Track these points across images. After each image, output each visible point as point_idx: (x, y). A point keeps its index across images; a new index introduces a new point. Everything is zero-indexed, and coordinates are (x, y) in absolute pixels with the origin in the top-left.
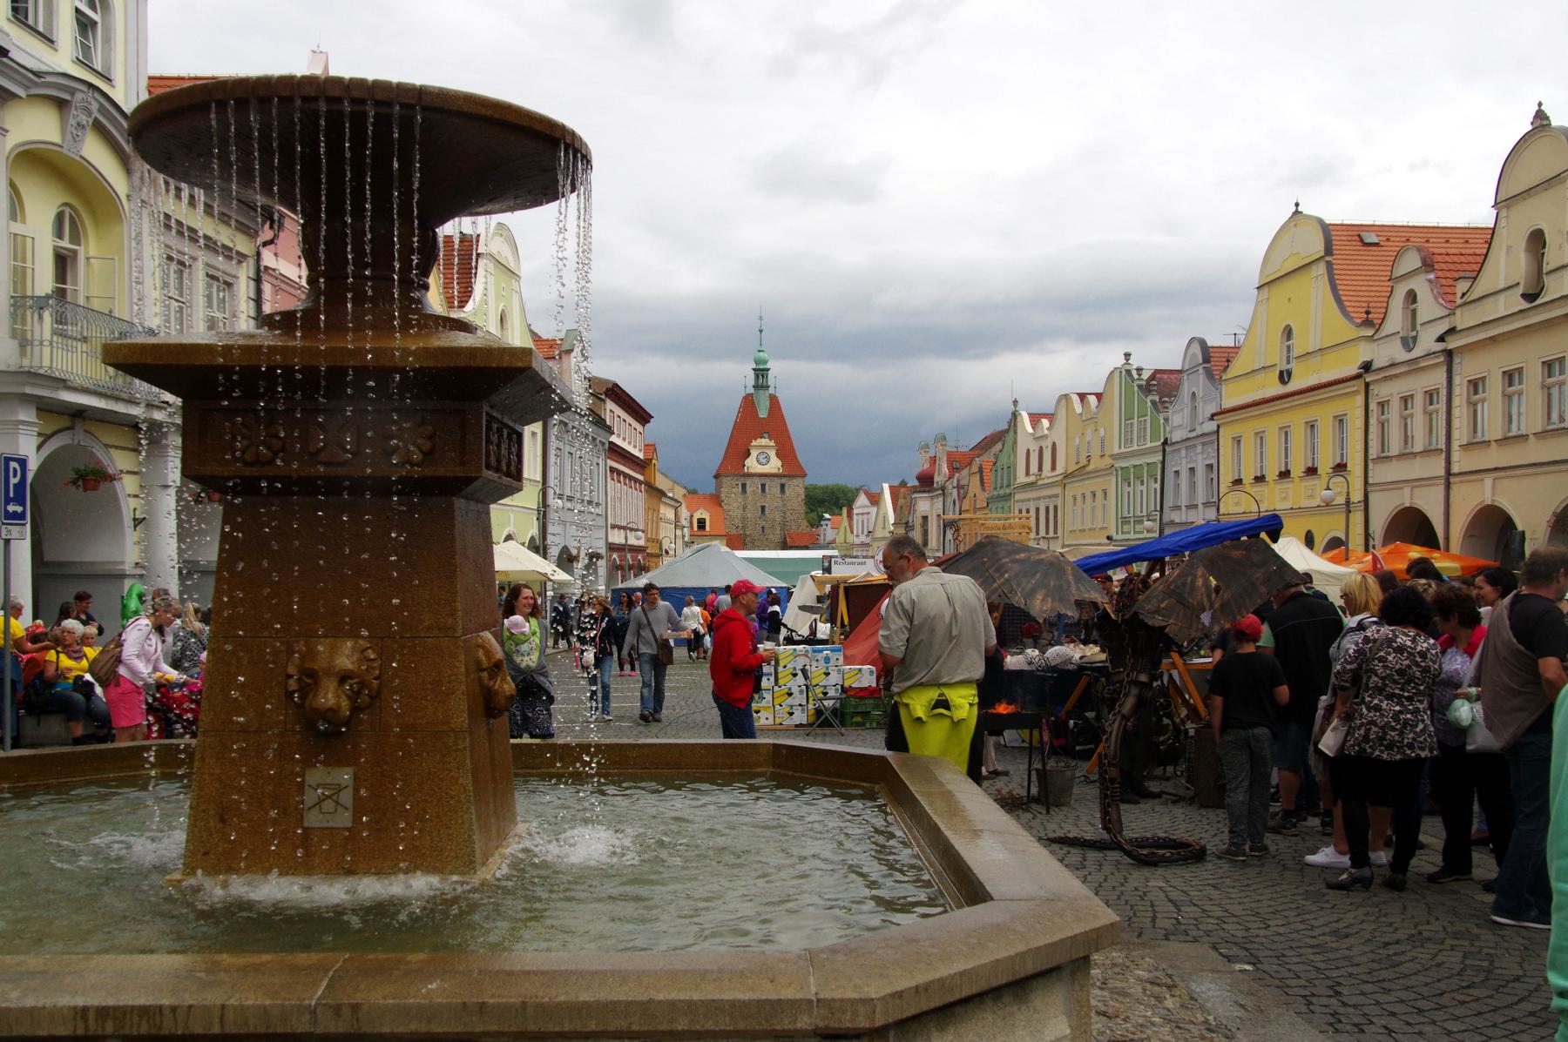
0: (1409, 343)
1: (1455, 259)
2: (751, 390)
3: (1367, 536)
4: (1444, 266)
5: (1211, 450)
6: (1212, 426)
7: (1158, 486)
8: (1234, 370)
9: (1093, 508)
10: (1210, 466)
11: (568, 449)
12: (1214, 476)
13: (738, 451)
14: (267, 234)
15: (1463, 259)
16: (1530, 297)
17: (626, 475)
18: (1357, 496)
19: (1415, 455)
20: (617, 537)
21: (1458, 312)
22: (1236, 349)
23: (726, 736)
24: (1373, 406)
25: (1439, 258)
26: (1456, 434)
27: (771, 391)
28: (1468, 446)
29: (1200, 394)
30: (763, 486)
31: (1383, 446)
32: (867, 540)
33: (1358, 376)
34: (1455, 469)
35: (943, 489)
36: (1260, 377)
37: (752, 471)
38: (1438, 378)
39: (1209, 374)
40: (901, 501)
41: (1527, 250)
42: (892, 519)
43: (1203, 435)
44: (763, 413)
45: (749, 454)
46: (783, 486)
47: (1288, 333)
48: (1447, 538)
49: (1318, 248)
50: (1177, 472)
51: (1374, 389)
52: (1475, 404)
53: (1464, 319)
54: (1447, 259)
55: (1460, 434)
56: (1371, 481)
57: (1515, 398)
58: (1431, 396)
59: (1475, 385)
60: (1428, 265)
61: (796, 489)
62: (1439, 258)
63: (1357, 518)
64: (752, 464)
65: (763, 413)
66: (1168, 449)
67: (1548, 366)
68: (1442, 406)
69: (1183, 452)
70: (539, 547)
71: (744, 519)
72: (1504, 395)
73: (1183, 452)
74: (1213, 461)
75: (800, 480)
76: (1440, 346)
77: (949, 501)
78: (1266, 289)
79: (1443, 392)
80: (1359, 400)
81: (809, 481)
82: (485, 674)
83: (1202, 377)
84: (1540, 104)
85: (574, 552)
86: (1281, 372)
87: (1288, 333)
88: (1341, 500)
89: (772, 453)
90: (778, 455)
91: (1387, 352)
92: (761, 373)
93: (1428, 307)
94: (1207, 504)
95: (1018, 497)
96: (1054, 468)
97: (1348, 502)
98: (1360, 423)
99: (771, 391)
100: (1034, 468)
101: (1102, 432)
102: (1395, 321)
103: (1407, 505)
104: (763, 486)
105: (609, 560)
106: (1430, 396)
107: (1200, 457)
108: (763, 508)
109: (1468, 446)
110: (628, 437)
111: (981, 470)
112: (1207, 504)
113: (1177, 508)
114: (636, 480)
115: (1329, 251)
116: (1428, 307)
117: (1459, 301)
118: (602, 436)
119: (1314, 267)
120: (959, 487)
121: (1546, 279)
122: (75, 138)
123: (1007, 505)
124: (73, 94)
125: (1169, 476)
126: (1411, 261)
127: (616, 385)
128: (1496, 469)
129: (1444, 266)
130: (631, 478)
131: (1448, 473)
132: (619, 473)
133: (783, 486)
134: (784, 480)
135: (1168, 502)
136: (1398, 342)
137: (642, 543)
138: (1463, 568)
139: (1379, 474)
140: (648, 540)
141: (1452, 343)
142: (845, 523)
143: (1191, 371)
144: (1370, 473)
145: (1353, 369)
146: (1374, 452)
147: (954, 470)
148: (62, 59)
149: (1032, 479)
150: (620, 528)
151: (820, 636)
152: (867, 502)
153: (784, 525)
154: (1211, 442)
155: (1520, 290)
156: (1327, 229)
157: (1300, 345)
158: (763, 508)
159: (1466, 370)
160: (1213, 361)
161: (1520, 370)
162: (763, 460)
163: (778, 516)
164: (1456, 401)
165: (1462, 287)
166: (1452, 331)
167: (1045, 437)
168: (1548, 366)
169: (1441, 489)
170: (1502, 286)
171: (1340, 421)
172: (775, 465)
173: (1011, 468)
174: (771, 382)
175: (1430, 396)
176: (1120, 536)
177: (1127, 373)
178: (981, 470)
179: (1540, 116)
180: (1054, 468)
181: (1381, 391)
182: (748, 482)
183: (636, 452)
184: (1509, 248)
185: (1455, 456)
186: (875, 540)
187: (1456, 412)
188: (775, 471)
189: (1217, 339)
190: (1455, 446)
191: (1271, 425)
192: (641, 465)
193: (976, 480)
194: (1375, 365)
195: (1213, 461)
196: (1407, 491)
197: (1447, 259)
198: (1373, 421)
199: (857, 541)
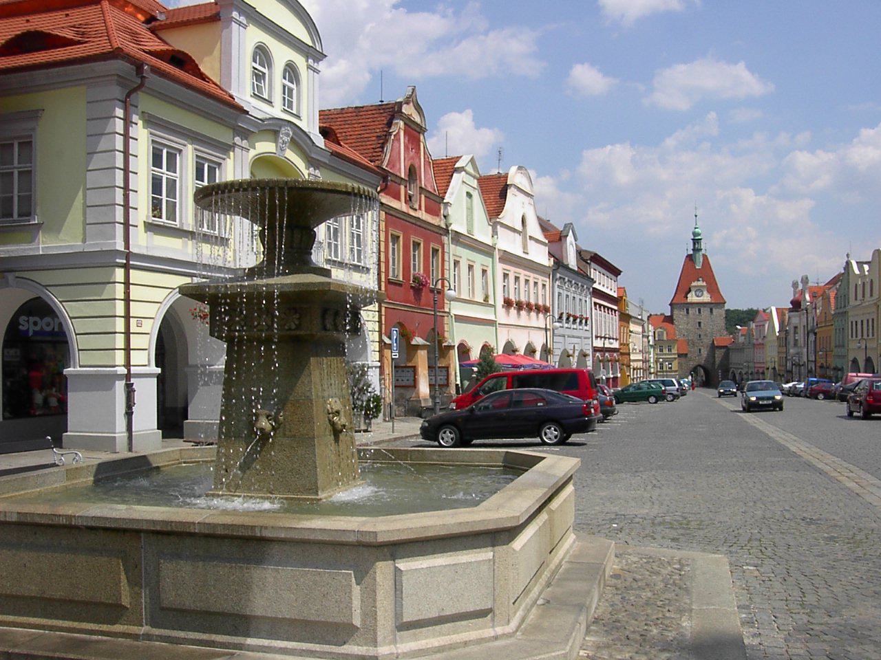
2: (691, 252)
11: (566, 293)
13: (683, 288)
20: (599, 343)
23: (115, 437)
42: (777, 329)
61: (719, 313)
81: (727, 307)
82: (331, 415)
85: (571, 352)
96: (871, 295)
100: (860, 296)
105: (594, 356)
108: (700, 323)
110: (604, 283)
122: (282, 150)
124: (281, 128)
127: (596, 254)
132: (600, 305)
138: (588, 371)
140: (621, 344)
144: (119, 351)
148: (277, 111)
149: (858, 303)
150: (601, 337)
180: (871, 295)
183: (612, 293)
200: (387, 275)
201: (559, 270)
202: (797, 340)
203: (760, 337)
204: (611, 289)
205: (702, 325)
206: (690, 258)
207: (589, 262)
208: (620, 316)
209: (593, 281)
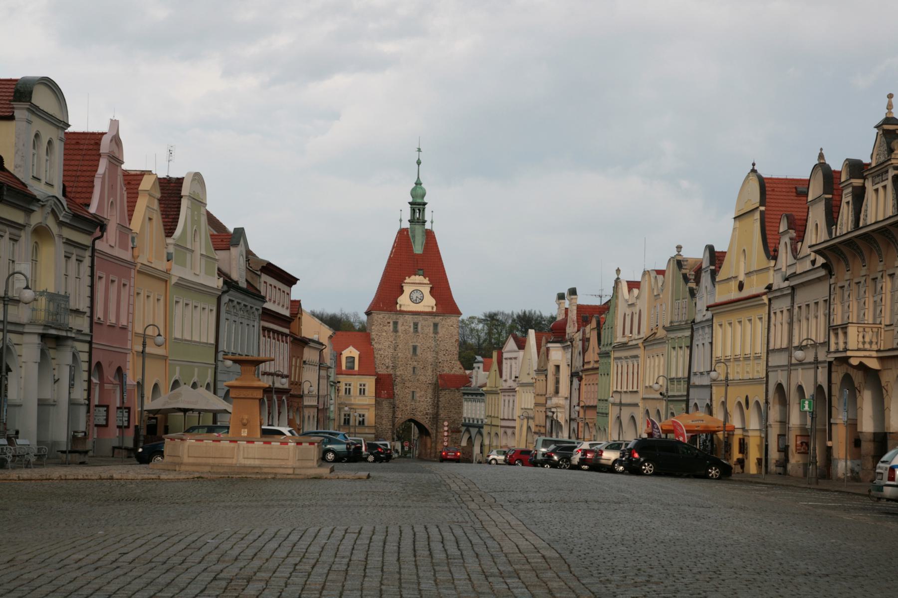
2: (406, 225)
11: (233, 318)
14: (98, 233)
17: (275, 331)
27: (428, 226)
30: (416, 325)
37: (403, 308)
44: (418, 249)
45: (402, 292)
46: (436, 325)
56: (770, 364)
64: (404, 302)
65: (418, 249)
70: (214, 388)
71: (395, 358)
77: (576, 352)
84: (821, 149)
88: (722, 377)
89: (426, 290)
92: (418, 206)
99: (428, 226)
104: (416, 325)
108: (415, 348)
114: (283, 334)
118: (257, 305)
122: (46, 218)
127: (269, 264)
130: (278, 333)
132: (269, 330)
133: (436, 325)
134: (437, 319)
137: (286, 386)
140: (291, 383)
144: (770, 359)
152: (515, 347)
158: (415, 348)
162: (416, 295)
163: (430, 356)
172: (429, 303)
174: (428, 217)
192: (284, 321)
199: (505, 386)
200: (644, 381)
201: (230, 292)
202: (830, 448)
203: (511, 378)
204: (283, 306)
205: (419, 351)
206: (403, 237)
207: (259, 273)
208: (292, 342)
209: (263, 299)
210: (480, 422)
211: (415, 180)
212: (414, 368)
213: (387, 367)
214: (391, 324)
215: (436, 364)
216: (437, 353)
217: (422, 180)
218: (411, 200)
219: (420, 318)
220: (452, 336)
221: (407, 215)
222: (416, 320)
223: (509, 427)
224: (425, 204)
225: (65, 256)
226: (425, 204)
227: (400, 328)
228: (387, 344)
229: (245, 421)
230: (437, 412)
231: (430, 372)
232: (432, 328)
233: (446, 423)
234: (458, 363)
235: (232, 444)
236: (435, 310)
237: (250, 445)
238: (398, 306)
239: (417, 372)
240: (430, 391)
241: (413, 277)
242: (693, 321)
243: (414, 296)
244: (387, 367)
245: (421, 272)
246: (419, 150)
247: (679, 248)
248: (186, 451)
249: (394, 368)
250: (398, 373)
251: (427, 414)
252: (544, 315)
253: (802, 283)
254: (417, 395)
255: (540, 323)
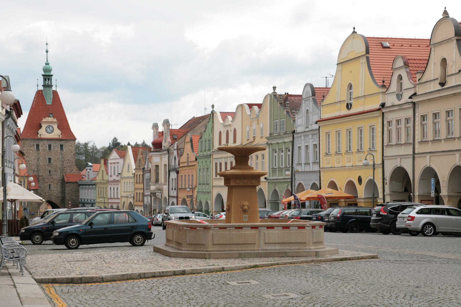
0: (399, 97)
1: (418, 62)
2: (41, 88)
3: (384, 179)
4: (413, 65)
5: (316, 138)
6: (316, 127)
7: (290, 153)
8: (326, 101)
9: (130, 187)
10: (315, 145)
12: (318, 150)
15: (421, 62)
16: (442, 84)
18: (379, 161)
19: (402, 145)
21: (417, 86)
22: (327, 90)
24: (385, 123)
25: (411, 61)
26: (417, 137)
27: (54, 88)
28: (421, 142)
29: (310, 111)
30: (50, 146)
31: (423, 134)
32: (118, 178)
33: (379, 109)
34: (416, 151)
35: (168, 150)
36: (338, 106)
37: (42, 137)
38: (410, 113)
39: (315, 101)
40: (140, 156)
41: (441, 65)
43: (312, 130)
44: (49, 102)
45: (40, 127)
46: (62, 146)
47: (350, 86)
48: (414, 180)
49: (363, 50)
50: (299, 147)
51: (386, 116)
52: (424, 125)
53: (420, 90)
54: (415, 62)
55: (418, 138)
56: (385, 155)
57: (437, 124)
58: (424, 117)
59: (423, 118)
60: (406, 64)
62: (411, 61)
63: (379, 172)
64: (43, 133)
65: (49, 102)
66: (295, 136)
67: (448, 112)
68: (411, 125)
69: (303, 138)
71: (38, 166)
72: (433, 123)
73: (303, 138)
74: (317, 143)
75: (72, 142)
76: (410, 100)
78: (341, 65)
79: (412, 119)
80: (380, 119)
83: (311, 103)
86: (347, 104)
87: (350, 86)
88: (371, 163)
89: (55, 126)
90: (59, 127)
91: (391, 100)
93: (407, 83)
94: (314, 163)
95: (215, 156)
97: (374, 165)
98: (380, 129)
99: (54, 88)
101: (261, 125)
102: (394, 87)
103: (399, 166)
104: (50, 146)
106: (407, 120)
107: (311, 140)
108: (50, 159)
109: (421, 142)
111: (191, 141)
112: (314, 163)
113: (300, 164)
115: (367, 52)
116: (407, 83)
117: (418, 82)
119: (361, 58)
120: (178, 149)
121: (447, 79)
123: (208, 160)
125: (296, 149)
126: (400, 63)
128: (430, 152)
129: (413, 65)
131: (414, 153)
133: (62, 146)
134: (62, 143)
135: (295, 162)
136: (395, 96)
139: (388, 152)
141: (415, 100)
142: (103, 168)
143: (307, 99)
144: (385, 152)
145: (377, 106)
146: (385, 144)
147: (174, 140)
151: (175, 195)
153: (62, 170)
154: (316, 134)
155: (438, 81)
156: (367, 41)
157: (356, 92)
158: (50, 159)
159: (421, 111)
160: (317, 94)
161: (452, 111)
163: (59, 164)
164: (417, 123)
165: (418, 76)
166: (415, 94)
167: (230, 125)
168: (448, 112)
169: (411, 159)
170: (432, 78)
171: (372, 129)
172: (57, 133)
173: (211, 141)
174: (53, 83)
175: (407, 120)
176: (271, 178)
177: (274, 95)
178: (191, 141)
179: (445, 13)
181: (389, 117)
182: (41, 144)
184: (435, 63)
185: (417, 146)
186: (122, 178)
187: (417, 128)
188: (57, 137)
189: (319, 83)
190: (416, 141)
191: (343, 127)
193: (188, 146)
194: (387, 105)
195: (317, 143)
196: (399, 160)
197: (415, 62)
198: (385, 129)
199: (111, 179)
206: (39, 94)
210: (92, 201)
211: (45, 62)
212: (50, 171)
213: (34, 171)
214: (35, 146)
215: (62, 169)
216: (63, 162)
217: (49, 62)
218: (43, 73)
219: (53, 142)
220: (71, 152)
221: (41, 82)
222: (50, 143)
223: (114, 203)
224: (52, 76)
225: (48, 64)
226: (52, 76)
227: (40, 148)
228: (33, 157)
229: (246, 207)
230: (64, 196)
231: (59, 173)
232: (59, 147)
233: (70, 202)
234: (75, 167)
235: (254, 231)
236: (61, 137)
237: (271, 231)
238: (39, 135)
239: (51, 173)
240: (59, 184)
241: (47, 118)
242: (294, 132)
243: (51, 128)
244: (34, 171)
245: (51, 115)
246: (47, 44)
247: (274, 88)
248: (210, 239)
249: (38, 171)
250: (40, 174)
251: (58, 197)
252: (80, 142)
253: (429, 99)
254: (52, 187)
255: (79, 147)
